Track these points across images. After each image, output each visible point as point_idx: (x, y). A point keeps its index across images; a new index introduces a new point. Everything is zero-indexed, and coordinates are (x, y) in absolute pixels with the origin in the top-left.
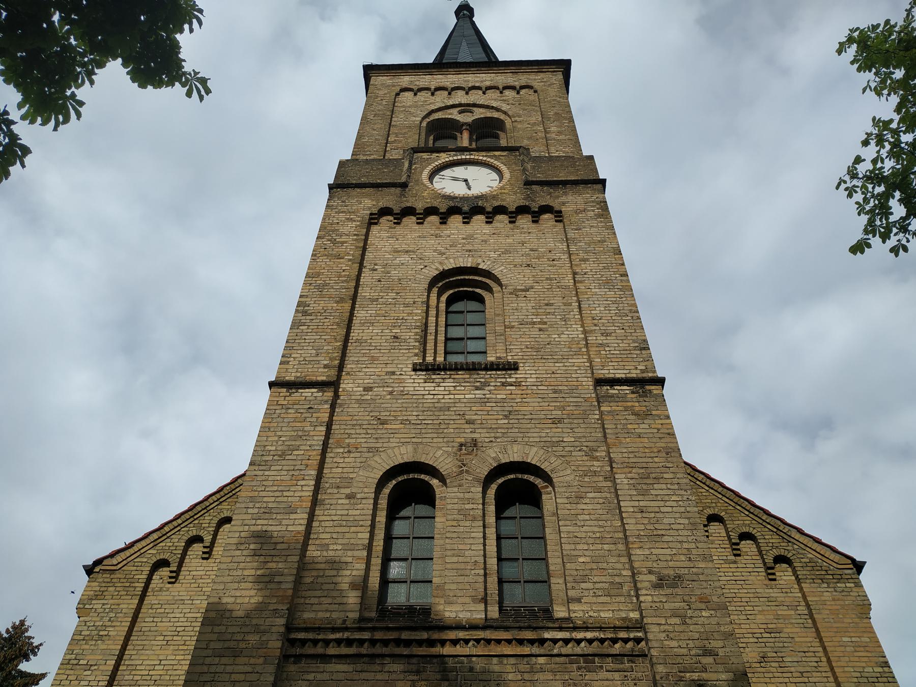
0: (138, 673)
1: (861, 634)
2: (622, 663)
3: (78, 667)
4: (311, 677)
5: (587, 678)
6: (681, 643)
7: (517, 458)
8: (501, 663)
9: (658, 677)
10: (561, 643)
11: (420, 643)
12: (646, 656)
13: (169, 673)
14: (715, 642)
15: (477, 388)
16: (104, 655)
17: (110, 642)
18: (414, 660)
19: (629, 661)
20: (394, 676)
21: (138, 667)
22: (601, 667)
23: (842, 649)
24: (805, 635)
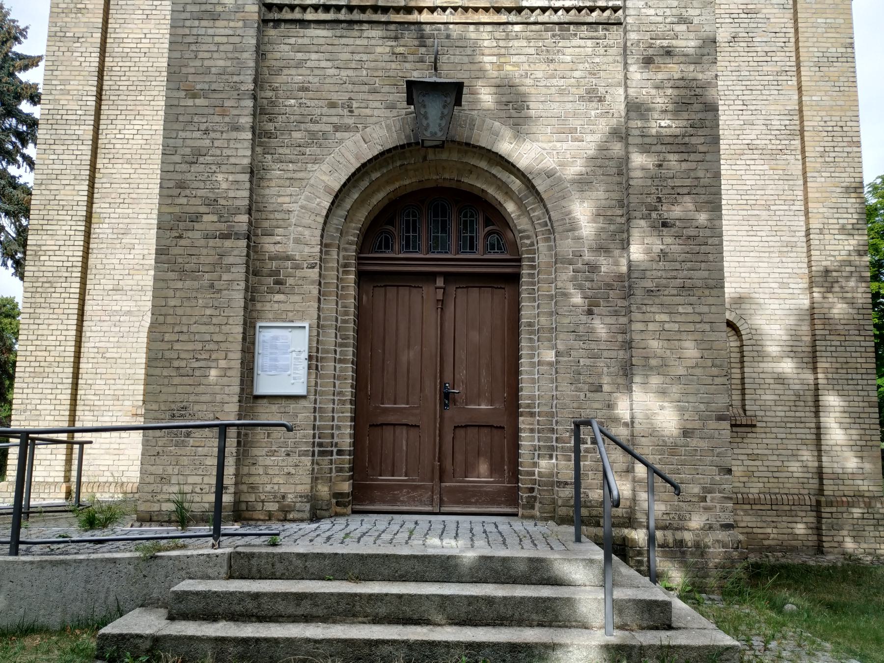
0: (126, 45)
1: (837, 16)
2: (596, 31)
3: (66, 39)
4: (292, 41)
5: (560, 45)
6: (658, 11)
8: (478, 30)
9: (629, 44)
10: (538, 11)
12: (621, 24)
13: (157, 46)
14: (692, 10)
16: (88, 28)
17: (89, 15)
18: (392, 27)
19: (603, 29)
20: (373, 42)
21: (125, 40)
22: (575, 35)
23: (814, 30)
24: (782, 16)
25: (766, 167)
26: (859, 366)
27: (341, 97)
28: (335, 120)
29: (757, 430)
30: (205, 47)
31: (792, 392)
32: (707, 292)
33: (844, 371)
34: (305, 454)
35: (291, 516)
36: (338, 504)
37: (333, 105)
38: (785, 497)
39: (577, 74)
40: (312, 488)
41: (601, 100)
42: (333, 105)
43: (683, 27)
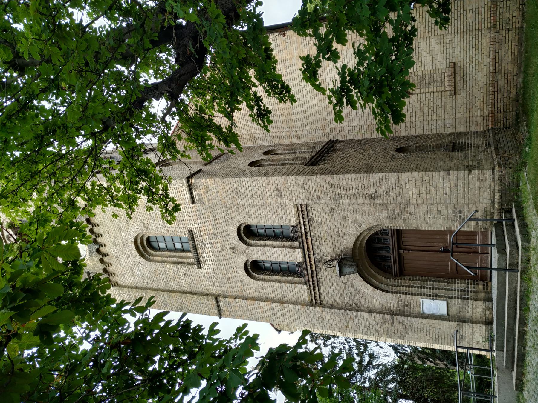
4: (326, 297)
7: (236, 234)
11: (311, 268)
15: (205, 246)
25: (328, 68)
26: (421, 17)
27: (342, 286)
28: (350, 287)
29: (456, 61)
30: (332, 322)
31: (436, 46)
32: (400, 179)
33: (424, 23)
34: (468, 303)
35: (491, 307)
36: (487, 289)
37: (345, 288)
38: (491, 46)
39: (325, 216)
40: (481, 300)
41: (333, 209)
42: (345, 288)
43: (305, 186)
